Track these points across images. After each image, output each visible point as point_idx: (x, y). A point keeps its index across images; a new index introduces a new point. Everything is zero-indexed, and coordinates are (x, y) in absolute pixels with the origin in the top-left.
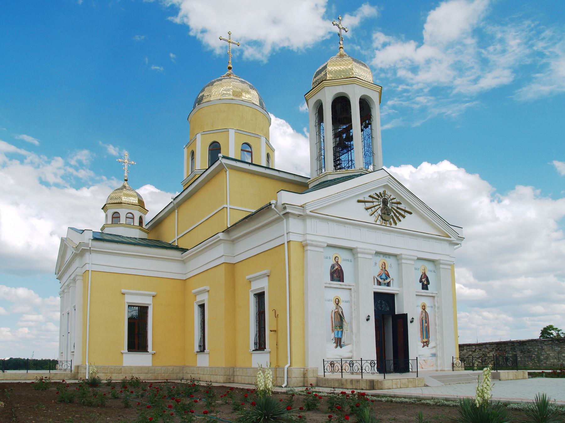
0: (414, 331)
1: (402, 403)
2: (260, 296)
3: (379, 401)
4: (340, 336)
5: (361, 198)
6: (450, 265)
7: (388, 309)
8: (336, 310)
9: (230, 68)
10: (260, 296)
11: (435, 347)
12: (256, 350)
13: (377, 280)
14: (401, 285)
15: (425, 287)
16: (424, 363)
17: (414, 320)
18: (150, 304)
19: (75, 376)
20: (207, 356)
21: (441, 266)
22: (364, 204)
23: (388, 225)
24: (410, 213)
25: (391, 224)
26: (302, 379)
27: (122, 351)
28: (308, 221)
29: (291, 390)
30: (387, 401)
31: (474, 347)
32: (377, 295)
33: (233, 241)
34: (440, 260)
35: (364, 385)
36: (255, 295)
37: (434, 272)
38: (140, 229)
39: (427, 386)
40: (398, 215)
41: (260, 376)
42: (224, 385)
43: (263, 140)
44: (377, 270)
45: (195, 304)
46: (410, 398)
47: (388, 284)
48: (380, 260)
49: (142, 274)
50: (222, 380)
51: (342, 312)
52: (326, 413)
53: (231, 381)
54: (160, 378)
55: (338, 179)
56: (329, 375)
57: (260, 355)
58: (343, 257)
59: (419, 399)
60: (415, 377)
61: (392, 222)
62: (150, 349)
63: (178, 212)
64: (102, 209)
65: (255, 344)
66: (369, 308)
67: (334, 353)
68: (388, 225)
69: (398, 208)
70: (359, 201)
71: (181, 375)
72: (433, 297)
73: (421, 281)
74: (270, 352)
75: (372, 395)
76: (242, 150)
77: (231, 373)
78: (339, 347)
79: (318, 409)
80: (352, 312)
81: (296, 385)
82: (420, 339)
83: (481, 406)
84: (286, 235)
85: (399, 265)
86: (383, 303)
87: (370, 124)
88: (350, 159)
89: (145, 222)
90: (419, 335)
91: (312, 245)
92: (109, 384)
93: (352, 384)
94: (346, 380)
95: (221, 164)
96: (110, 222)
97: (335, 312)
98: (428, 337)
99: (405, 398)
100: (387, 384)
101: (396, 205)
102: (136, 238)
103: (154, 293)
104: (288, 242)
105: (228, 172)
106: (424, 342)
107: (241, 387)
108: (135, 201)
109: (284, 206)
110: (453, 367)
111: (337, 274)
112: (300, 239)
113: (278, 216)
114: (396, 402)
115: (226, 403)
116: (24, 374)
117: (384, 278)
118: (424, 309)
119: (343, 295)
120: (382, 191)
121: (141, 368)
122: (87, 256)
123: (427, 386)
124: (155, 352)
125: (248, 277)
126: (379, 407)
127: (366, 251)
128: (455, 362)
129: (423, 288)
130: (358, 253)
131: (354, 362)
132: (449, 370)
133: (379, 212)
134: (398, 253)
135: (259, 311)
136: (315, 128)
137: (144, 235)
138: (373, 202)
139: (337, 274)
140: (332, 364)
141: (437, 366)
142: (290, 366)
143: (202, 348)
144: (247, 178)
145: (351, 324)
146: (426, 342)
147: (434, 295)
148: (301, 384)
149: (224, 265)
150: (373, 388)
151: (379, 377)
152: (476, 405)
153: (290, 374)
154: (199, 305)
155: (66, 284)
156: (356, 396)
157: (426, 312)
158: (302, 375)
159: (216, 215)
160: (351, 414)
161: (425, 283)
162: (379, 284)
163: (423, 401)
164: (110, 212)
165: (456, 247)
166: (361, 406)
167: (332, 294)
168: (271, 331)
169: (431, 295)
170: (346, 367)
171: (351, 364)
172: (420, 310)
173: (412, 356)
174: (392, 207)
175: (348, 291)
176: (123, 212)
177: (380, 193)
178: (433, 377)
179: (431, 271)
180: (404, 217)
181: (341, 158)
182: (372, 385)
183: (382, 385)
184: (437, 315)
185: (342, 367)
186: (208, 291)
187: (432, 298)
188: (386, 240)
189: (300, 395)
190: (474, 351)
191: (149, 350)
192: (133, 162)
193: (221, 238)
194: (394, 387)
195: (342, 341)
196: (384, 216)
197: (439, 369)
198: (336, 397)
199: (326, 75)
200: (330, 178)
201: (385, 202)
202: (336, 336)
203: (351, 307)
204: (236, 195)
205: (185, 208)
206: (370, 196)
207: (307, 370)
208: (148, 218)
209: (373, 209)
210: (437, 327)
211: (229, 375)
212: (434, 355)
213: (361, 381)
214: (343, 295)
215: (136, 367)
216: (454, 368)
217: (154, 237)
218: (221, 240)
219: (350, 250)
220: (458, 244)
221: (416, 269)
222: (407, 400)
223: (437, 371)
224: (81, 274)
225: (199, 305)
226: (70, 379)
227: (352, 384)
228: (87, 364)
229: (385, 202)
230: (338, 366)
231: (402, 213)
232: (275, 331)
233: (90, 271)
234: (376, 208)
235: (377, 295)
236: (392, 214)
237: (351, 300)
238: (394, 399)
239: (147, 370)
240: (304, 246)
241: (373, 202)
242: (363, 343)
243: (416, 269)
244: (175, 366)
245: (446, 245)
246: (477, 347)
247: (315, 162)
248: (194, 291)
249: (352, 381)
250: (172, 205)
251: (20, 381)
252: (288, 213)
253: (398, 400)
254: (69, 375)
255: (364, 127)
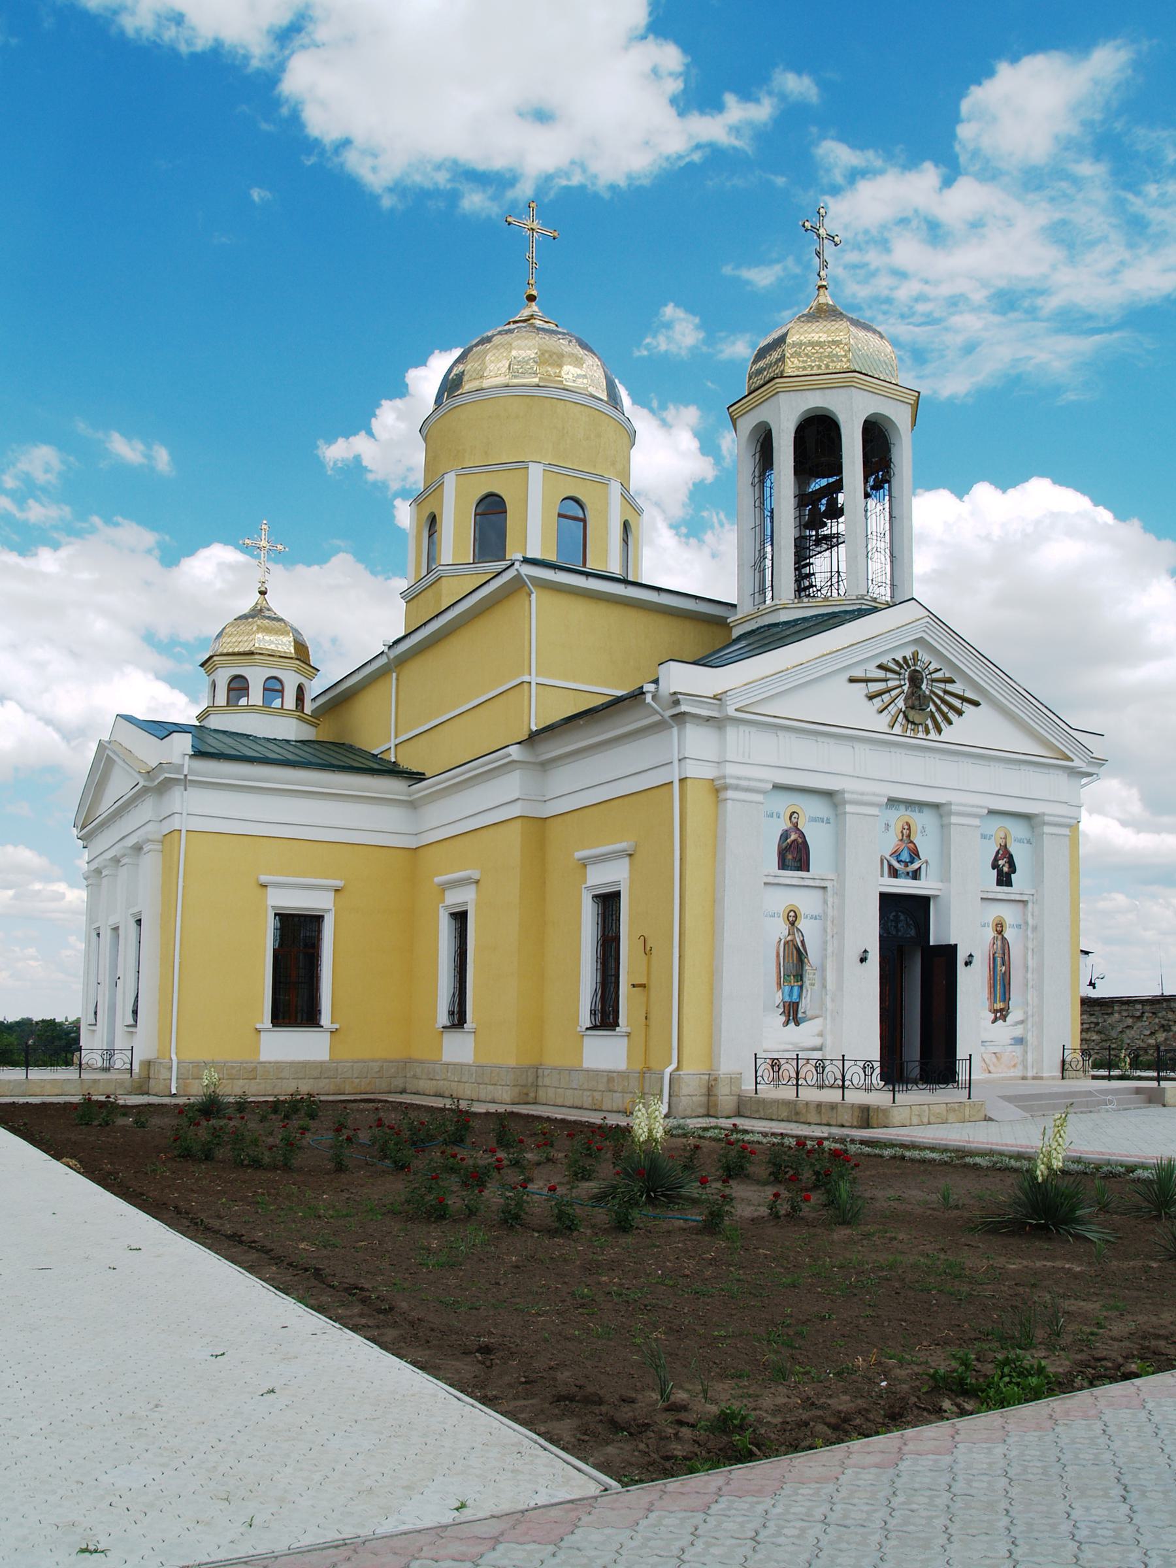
0: (971, 987)
1: (923, 1161)
2: (608, 902)
3: (875, 1155)
4: (795, 998)
5: (858, 673)
6: (1069, 826)
7: (913, 933)
8: (789, 938)
9: (531, 298)
10: (608, 902)
11: (1022, 1022)
12: (594, 1028)
13: (890, 866)
14: (945, 877)
15: (1004, 879)
16: (995, 1060)
17: (975, 961)
18: (329, 910)
19: (141, 1087)
20: (471, 1038)
21: (1047, 829)
22: (864, 685)
23: (921, 735)
24: (976, 704)
25: (927, 732)
26: (704, 1099)
27: (258, 1026)
28: (731, 732)
29: (679, 1127)
30: (894, 1157)
31: (1139, 1006)
32: (887, 900)
33: (545, 766)
34: (1044, 814)
35: (846, 1118)
36: (595, 897)
37: (1029, 842)
38: (300, 718)
39: (991, 1119)
40: (945, 709)
41: (639, 1114)
42: (516, 1109)
43: (615, 488)
44: (890, 842)
45: (441, 911)
46: (945, 1150)
47: (916, 875)
48: (897, 817)
49: (303, 835)
50: (507, 1097)
51: (803, 942)
52: (765, 1184)
53: (530, 1099)
54: (348, 1089)
55: (805, 619)
56: (767, 1092)
57: (609, 1040)
58: (810, 811)
59: (962, 1153)
60: (964, 1099)
61: (931, 727)
62: (325, 1019)
63: (397, 679)
64: (202, 665)
65: (593, 1013)
66: (866, 931)
67: (780, 1039)
68: (921, 735)
69: (946, 692)
70: (852, 680)
71: (399, 1083)
72: (1024, 902)
73: (995, 865)
74: (628, 1035)
75: (862, 1142)
76: (560, 515)
77: (530, 1080)
78: (792, 1025)
79: (747, 1176)
80: (825, 942)
81: (688, 1112)
82: (987, 1003)
83: (1045, 1181)
84: (676, 762)
85: (944, 827)
86: (902, 917)
87: (889, 482)
88: (835, 569)
89: (308, 696)
90: (984, 993)
91: (737, 788)
92: (242, 1106)
93: (820, 1113)
94: (807, 1104)
95: (518, 577)
96: (221, 700)
97: (787, 943)
98: (1006, 997)
99: (932, 1149)
100: (898, 1116)
101: (942, 685)
102: (288, 741)
103: (338, 883)
104: (682, 780)
105: (533, 596)
106: (995, 1011)
107: (559, 1117)
108: (285, 644)
109: (674, 698)
110: (1063, 1069)
111: (794, 854)
112: (709, 772)
113: (657, 718)
114: (912, 1160)
115: (549, 1160)
116: (18, 1083)
117: (907, 860)
118: (1000, 933)
119: (807, 903)
120: (909, 655)
121: (305, 1065)
122: (177, 792)
123: (991, 1119)
124: (337, 1026)
125: (579, 854)
126: (874, 1172)
127: (865, 798)
128: (1068, 1059)
129: (1000, 883)
130: (845, 802)
131: (827, 1063)
132: (1053, 1078)
133: (900, 703)
134: (944, 802)
135: (603, 935)
136: (751, 489)
137: (306, 732)
138: (886, 680)
139: (794, 854)
140: (775, 1064)
141: (1025, 1067)
142: (678, 1069)
143: (458, 1018)
144: (579, 610)
145: (824, 970)
146: (1001, 1010)
147: (1025, 898)
148: (702, 1111)
149: (519, 821)
150: (867, 1125)
151: (880, 1098)
152: (1036, 1178)
153: (676, 1088)
154: (452, 914)
155: (109, 855)
156: (826, 1155)
157: (1003, 939)
158: (704, 1091)
159: (501, 697)
160: (816, 1187)
161: (1006, 869)
162: (894, 873)
163: (968, 1160)
164: (223, 677)
165: (1084, 781)
166: (834, 1176)
167: (781, 900)
168: (634, 986)
169: (1018, 897)
170: (808, 1071)
171: (820, 1066)
172: (990, 933)
173: (961, 1053)
174: (932, 692)
175: (819, 893)
176: (256, 677)
177: (904, 658)
178: (1008, 1099)
179: (1020, 841)
180: (960, 713)
181: (812, 560)
182: (866, 1116)
183: (887, 1118)
184: (1030, 946)
185: (797, 1074)
186: (477, 882)
187: (1021, 905)
188: (916, 771)
189: (700, 1137)
190: (1140, 1018)
191: (322, 1023)
192: (280, 547)
193: (515, 757)
194: (915, 1121)
195: (801, 1010)
196: (912, 715)
197: (1030, 1074)
198: (785, 1153)
199: (782, 359)
200: (784, 616)
201: (915, 680)
202: (787, 999)
203: (825, 930)
204: (557, 656)
205: (414, 669)
206: (880, 667)
207: (716, 1080)
208: (315, 687)
209: (886, 697)
210: (1030, 975)
211: (524, 1086)
212: (1020, 1041)
213: (840, 1108)
214: (807, 903)
215: (292, 1063)
216: (1067, 1073)
217: (334, 743)
218: (513, 761)
219: (828, 794)
220: (1091, 775)
221: (984, 837)
222: (934, 1155)
223: (1024, 1078)
224: (159, 837)
225: (452, 914)
226: (129, 1094)
227: (820, 1113)
228: (174, 1057)
229: (915, 680)
230: (789, 1070)
231: (957, 703)
232: (643, 986)
233: (184, 832)
234: (894, 693)
235: (887, 900)
236: (932, 707)
237: (825, 913)
238: (907, 1154)
239: (302, 1068)
240: (717, 789)
241: (886, 680)
242: (850, 1017)
243: (984, 837)
244: (386, 1061)
245: (1061, 779)
246: (1147, 1008)
247: (749, 573)
248: (438, 879)
249: (819, 1106)
250: (383, 660)
251: (16, 1100)
252: (684, 713)
253: (916, 1154)
254: (128, 1084)
255: (873, 488)
